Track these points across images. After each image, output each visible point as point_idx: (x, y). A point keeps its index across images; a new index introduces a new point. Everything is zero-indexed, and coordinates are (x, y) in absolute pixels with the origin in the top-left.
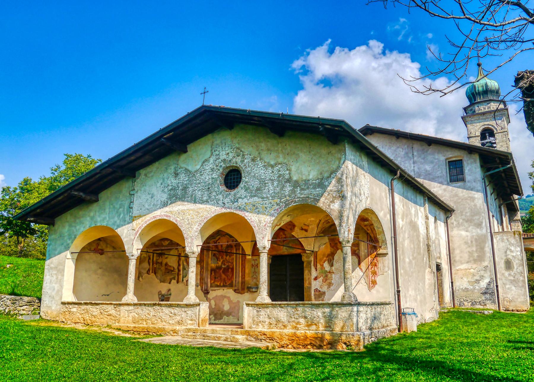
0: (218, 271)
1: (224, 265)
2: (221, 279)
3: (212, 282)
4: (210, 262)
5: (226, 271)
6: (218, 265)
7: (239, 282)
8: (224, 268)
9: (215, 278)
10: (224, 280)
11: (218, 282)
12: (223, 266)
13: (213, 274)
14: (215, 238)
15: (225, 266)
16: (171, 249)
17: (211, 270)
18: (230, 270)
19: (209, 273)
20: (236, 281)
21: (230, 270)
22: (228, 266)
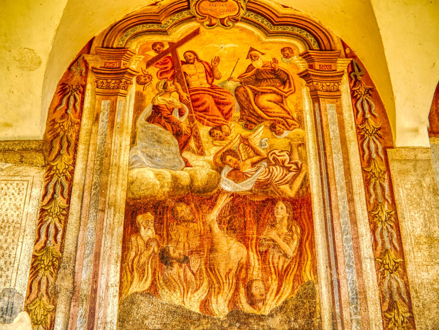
0: (183, 210)
1: (237, 174)
2: (211, 267)
3: (139, 286)
4: (124, 158)
5: (251, 213)
6: (184, 176)
7: (360, 295)
8: (235, 196)
9: (164, 258)
10: (242, 278)
11: (187, 287)
12: (228, 185)
13: (147, 232)
14: (164, 32)
15: (245, 187)
16: (276, 275)
17: (133, 209)
18: (282, 211)
19: (116, 221)
20: (334, 286)
21: (282, 211)
22: (262, 186)
